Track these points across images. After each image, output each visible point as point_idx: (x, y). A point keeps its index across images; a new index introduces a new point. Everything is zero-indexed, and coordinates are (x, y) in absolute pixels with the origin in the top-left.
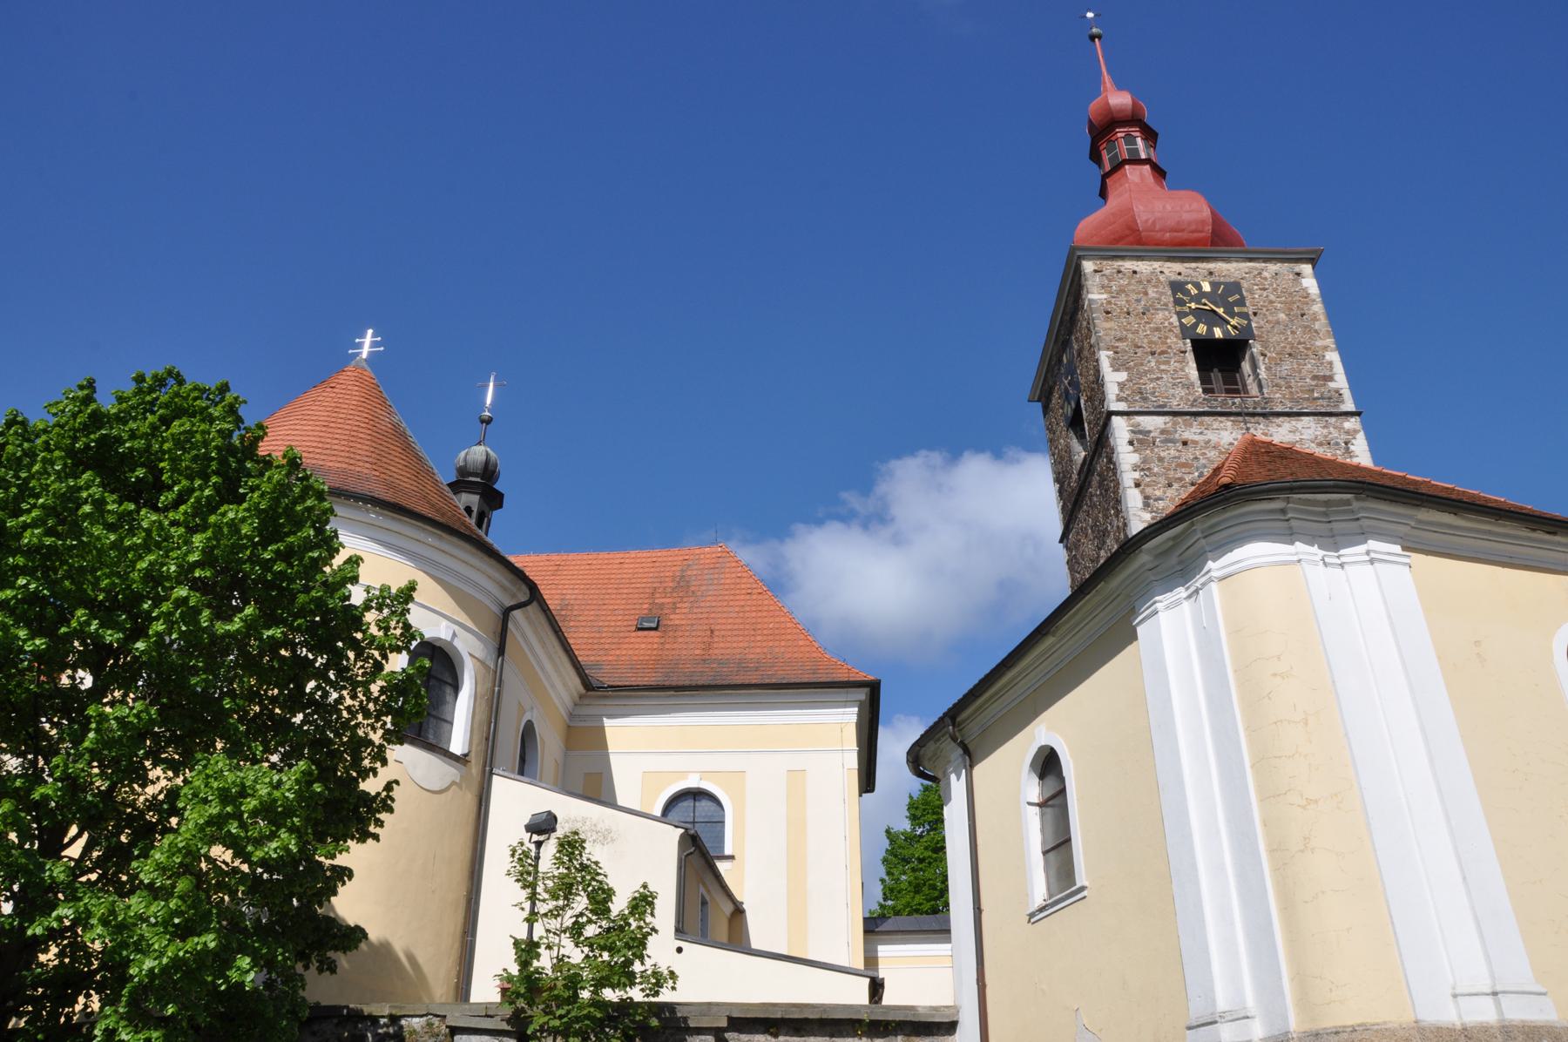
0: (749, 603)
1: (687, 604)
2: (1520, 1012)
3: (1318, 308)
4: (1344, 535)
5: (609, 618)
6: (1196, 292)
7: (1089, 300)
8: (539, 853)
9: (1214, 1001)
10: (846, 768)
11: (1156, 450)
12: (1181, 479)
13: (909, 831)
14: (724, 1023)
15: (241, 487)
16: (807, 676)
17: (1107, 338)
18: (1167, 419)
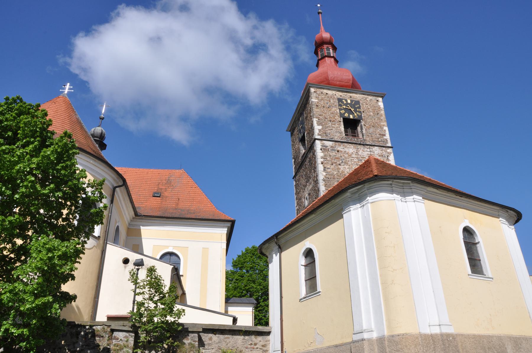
0: (191, 190)
1: (170, 189)
2: (446, 330)
3: (383, 112)
4: (407, 193)
5: (143, 192)
6: (346, 103)
7: (312, 101)
8: (138, 272)
9: (362, 327)
10: (222, 248)
11: (329, 152)
12: (336, 163)
14: (201, 330)
15: (47, 142)
16: (211, 217)
17: (316, 114)
18: (333, 143)
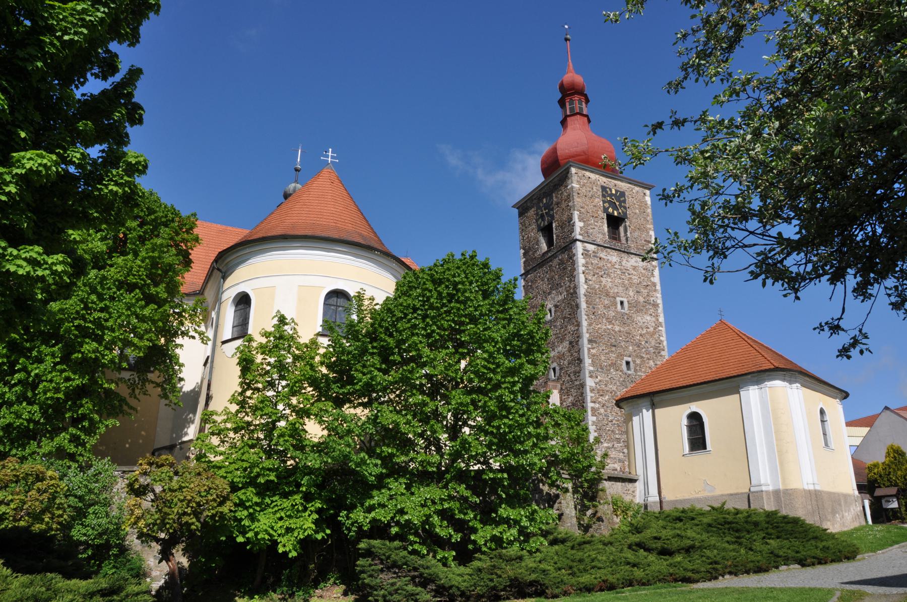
2: (818, 488)
3: (649, 211)
18: (595, 247)
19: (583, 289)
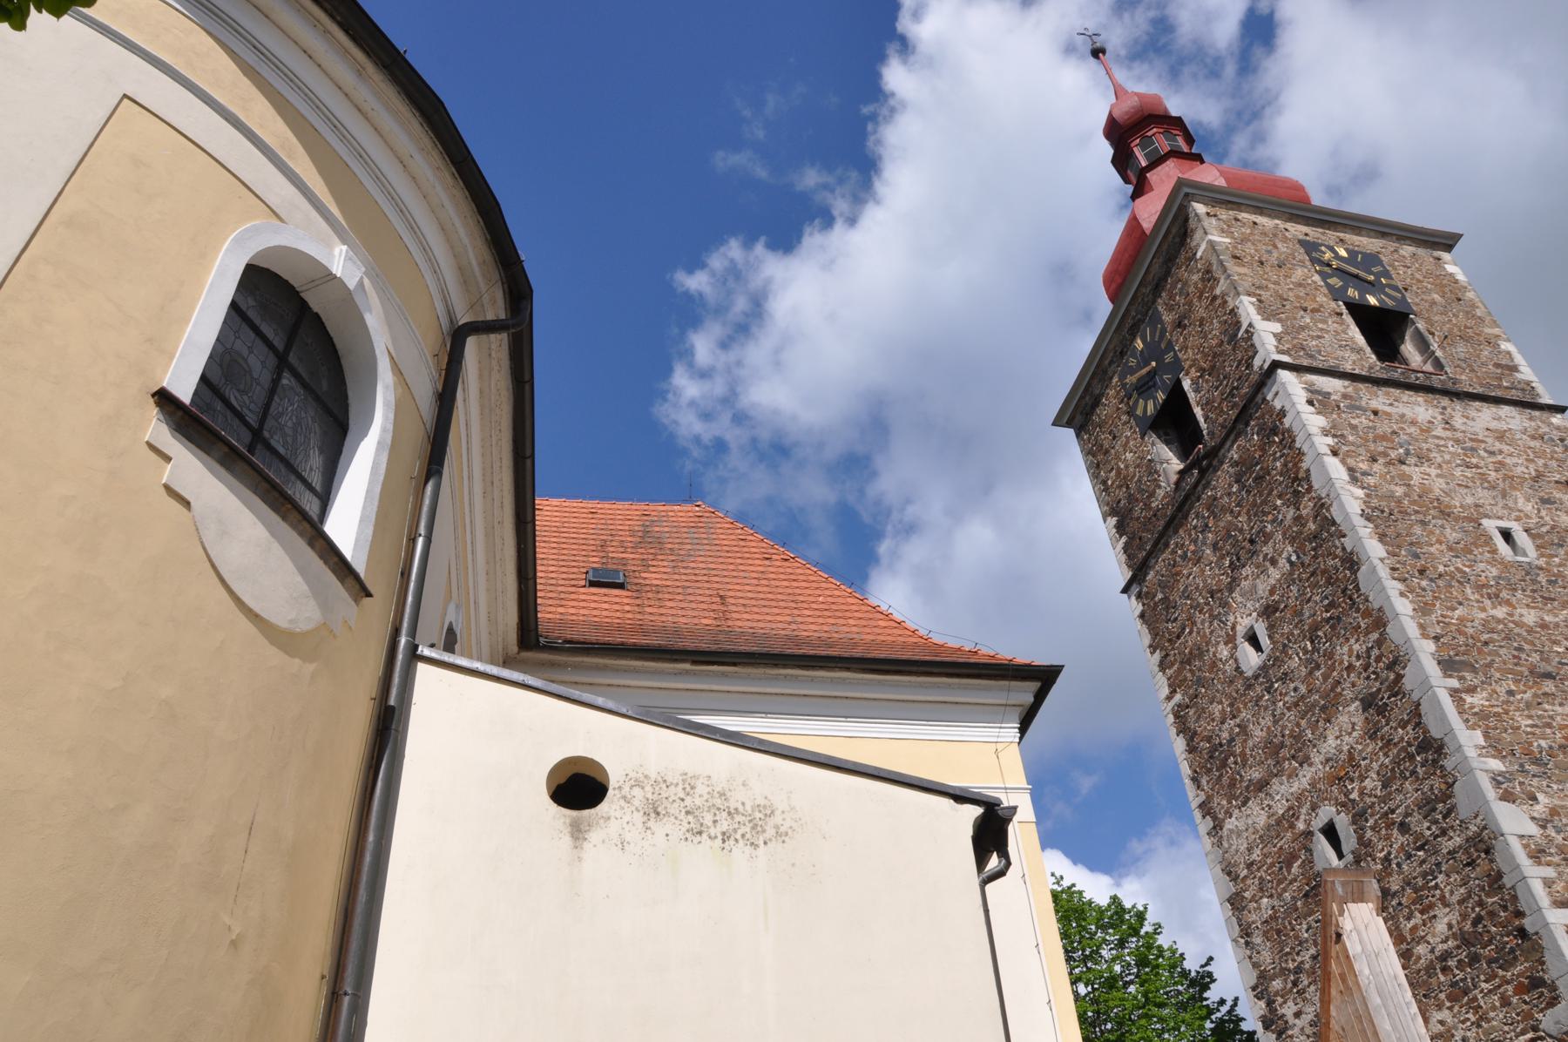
12: (1385, 455)
13: (1119, 972)
19: (1350, 502)
